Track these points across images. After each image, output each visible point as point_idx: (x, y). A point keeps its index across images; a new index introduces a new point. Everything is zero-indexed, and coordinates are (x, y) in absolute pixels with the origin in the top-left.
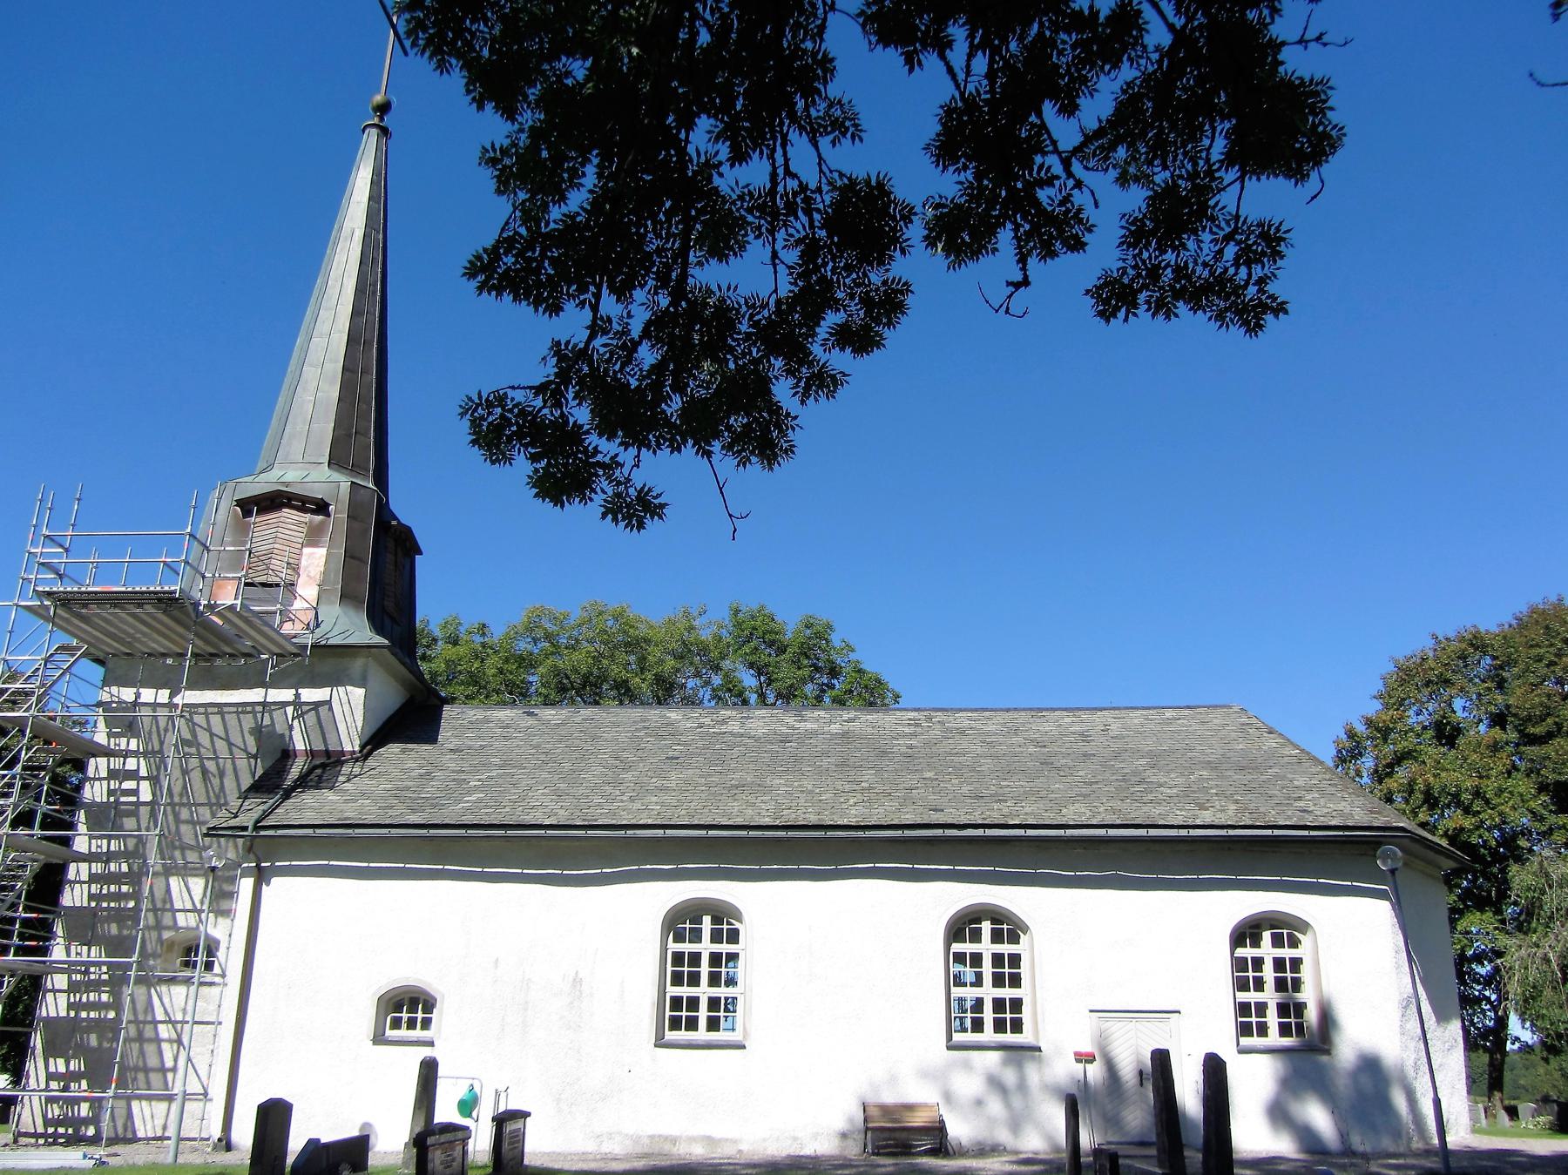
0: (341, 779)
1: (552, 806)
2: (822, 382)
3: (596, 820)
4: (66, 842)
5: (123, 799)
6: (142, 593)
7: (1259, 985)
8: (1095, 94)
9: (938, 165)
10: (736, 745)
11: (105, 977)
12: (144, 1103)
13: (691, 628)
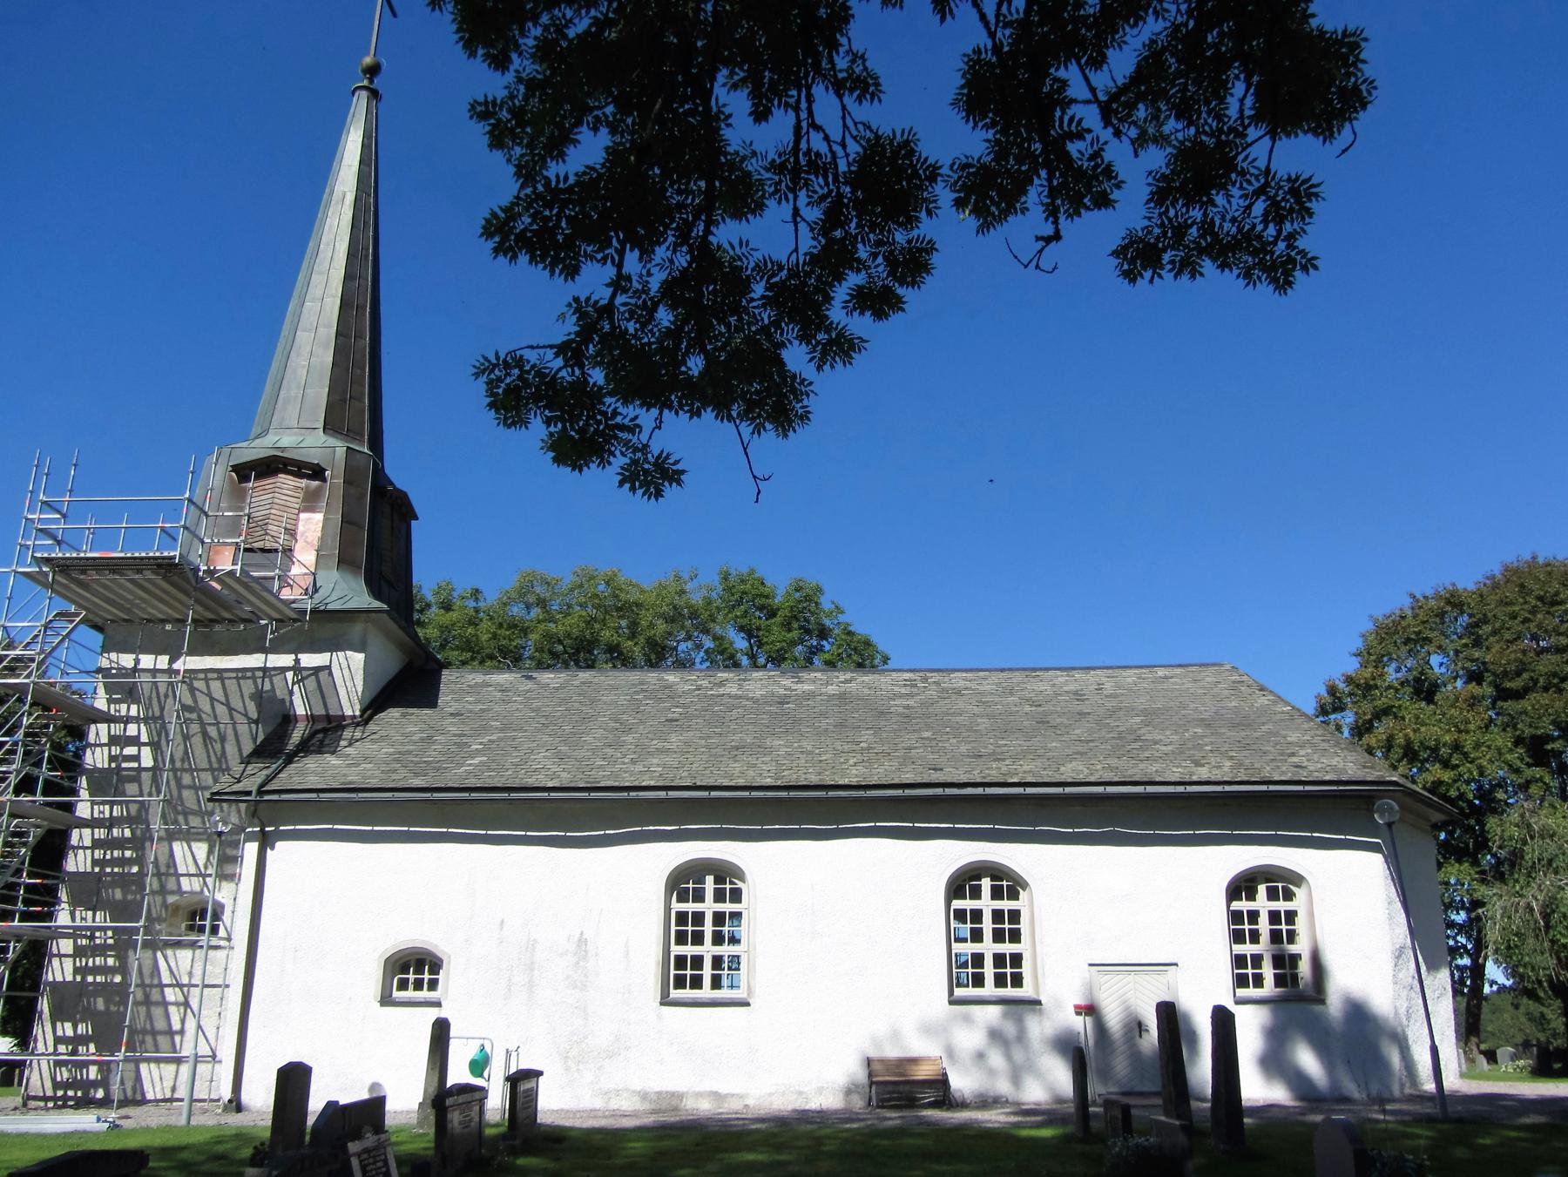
0: (343, 743)
1: (555, 768)
2: (841, 347)
3: (599, 782)
4: (69, 808)
5: (124, 765)
6: (142, 558)
7: (1255, 936)
8: (1124, 46)
9: (968, 121)
10: (734, 707)
11: (110, 941)
12: (153, 1066)
13: (683, 592)
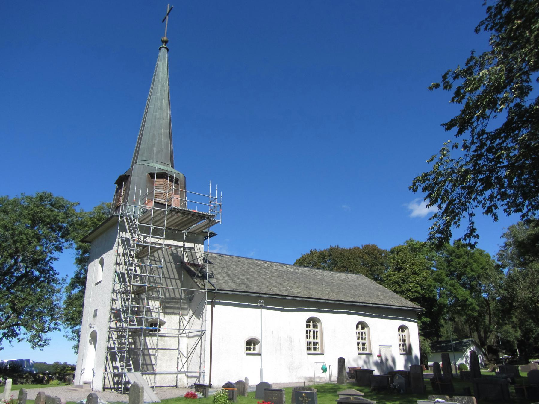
12: (147, 376)
